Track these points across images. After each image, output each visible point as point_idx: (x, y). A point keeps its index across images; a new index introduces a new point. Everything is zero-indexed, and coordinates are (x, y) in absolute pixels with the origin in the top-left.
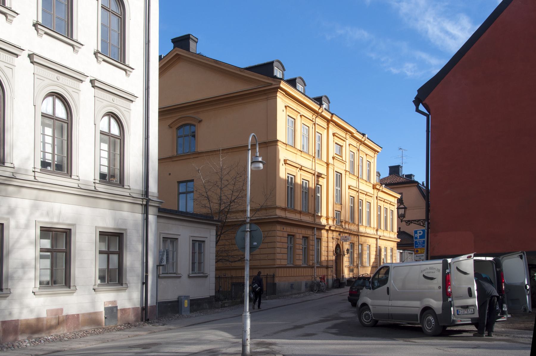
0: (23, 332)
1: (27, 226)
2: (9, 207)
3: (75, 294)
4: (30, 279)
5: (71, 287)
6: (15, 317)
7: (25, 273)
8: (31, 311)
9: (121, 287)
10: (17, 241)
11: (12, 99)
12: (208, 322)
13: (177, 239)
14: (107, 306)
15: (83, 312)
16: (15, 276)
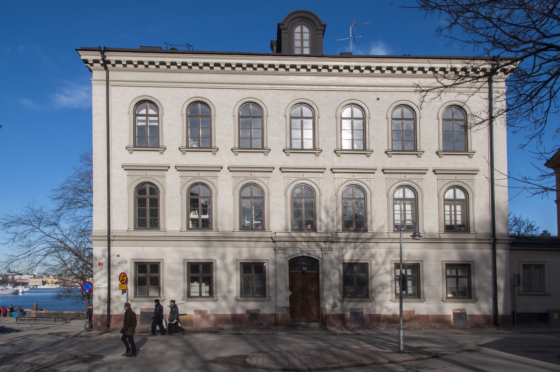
0: (383, 322)
1: (384, 263)
2: (371, 254)
3: (424, 303)
4: (387, 293)
5: (421, 299)
6: (378, 312)
7: (383, 289)
8: (389, 310)
9: (471, 300)
10: (377, 272)
11: (217, 194)
12: (549, 333)
13: (544, 265)
14: (455, 312)
15: (432, 314)
16: (377, 290)
